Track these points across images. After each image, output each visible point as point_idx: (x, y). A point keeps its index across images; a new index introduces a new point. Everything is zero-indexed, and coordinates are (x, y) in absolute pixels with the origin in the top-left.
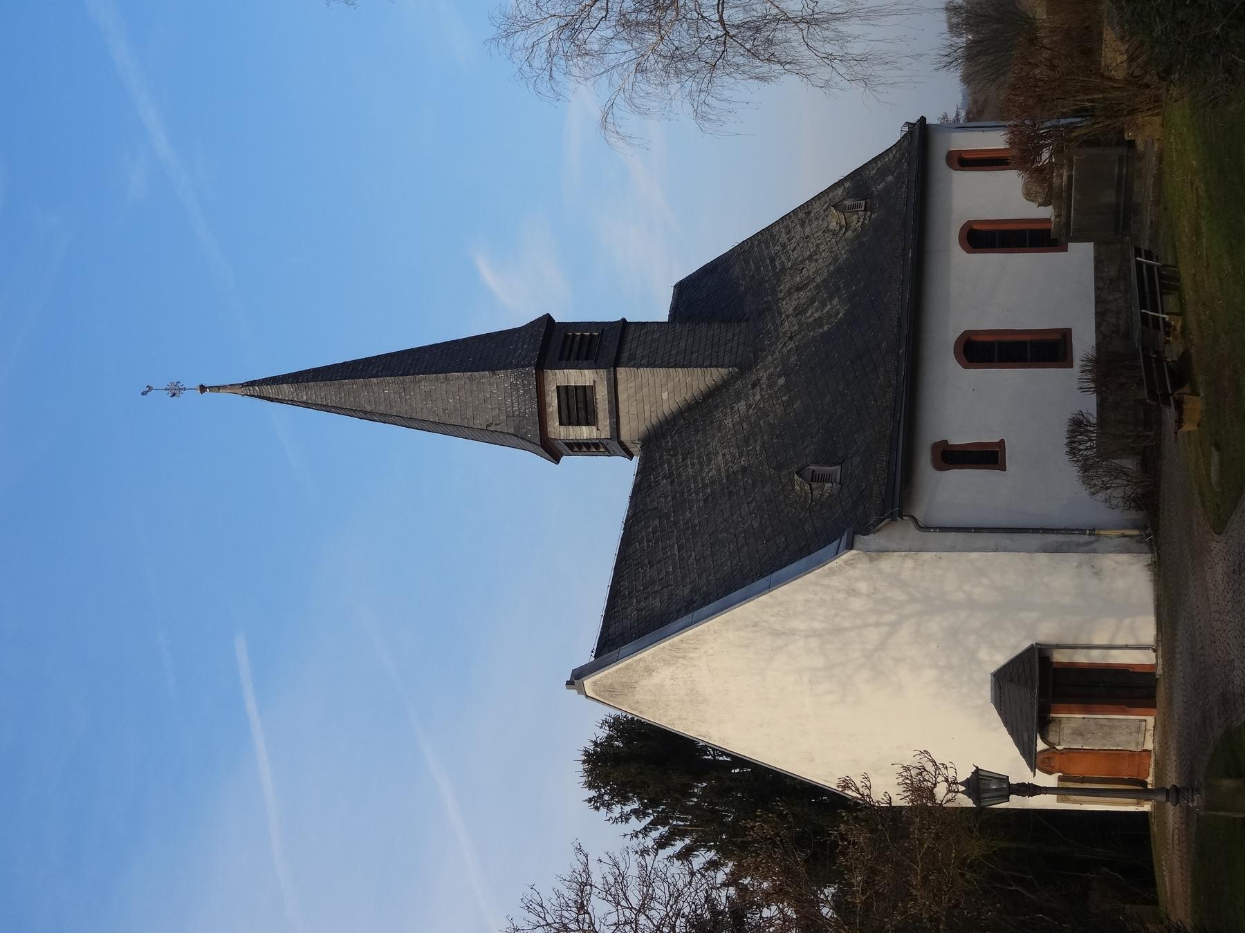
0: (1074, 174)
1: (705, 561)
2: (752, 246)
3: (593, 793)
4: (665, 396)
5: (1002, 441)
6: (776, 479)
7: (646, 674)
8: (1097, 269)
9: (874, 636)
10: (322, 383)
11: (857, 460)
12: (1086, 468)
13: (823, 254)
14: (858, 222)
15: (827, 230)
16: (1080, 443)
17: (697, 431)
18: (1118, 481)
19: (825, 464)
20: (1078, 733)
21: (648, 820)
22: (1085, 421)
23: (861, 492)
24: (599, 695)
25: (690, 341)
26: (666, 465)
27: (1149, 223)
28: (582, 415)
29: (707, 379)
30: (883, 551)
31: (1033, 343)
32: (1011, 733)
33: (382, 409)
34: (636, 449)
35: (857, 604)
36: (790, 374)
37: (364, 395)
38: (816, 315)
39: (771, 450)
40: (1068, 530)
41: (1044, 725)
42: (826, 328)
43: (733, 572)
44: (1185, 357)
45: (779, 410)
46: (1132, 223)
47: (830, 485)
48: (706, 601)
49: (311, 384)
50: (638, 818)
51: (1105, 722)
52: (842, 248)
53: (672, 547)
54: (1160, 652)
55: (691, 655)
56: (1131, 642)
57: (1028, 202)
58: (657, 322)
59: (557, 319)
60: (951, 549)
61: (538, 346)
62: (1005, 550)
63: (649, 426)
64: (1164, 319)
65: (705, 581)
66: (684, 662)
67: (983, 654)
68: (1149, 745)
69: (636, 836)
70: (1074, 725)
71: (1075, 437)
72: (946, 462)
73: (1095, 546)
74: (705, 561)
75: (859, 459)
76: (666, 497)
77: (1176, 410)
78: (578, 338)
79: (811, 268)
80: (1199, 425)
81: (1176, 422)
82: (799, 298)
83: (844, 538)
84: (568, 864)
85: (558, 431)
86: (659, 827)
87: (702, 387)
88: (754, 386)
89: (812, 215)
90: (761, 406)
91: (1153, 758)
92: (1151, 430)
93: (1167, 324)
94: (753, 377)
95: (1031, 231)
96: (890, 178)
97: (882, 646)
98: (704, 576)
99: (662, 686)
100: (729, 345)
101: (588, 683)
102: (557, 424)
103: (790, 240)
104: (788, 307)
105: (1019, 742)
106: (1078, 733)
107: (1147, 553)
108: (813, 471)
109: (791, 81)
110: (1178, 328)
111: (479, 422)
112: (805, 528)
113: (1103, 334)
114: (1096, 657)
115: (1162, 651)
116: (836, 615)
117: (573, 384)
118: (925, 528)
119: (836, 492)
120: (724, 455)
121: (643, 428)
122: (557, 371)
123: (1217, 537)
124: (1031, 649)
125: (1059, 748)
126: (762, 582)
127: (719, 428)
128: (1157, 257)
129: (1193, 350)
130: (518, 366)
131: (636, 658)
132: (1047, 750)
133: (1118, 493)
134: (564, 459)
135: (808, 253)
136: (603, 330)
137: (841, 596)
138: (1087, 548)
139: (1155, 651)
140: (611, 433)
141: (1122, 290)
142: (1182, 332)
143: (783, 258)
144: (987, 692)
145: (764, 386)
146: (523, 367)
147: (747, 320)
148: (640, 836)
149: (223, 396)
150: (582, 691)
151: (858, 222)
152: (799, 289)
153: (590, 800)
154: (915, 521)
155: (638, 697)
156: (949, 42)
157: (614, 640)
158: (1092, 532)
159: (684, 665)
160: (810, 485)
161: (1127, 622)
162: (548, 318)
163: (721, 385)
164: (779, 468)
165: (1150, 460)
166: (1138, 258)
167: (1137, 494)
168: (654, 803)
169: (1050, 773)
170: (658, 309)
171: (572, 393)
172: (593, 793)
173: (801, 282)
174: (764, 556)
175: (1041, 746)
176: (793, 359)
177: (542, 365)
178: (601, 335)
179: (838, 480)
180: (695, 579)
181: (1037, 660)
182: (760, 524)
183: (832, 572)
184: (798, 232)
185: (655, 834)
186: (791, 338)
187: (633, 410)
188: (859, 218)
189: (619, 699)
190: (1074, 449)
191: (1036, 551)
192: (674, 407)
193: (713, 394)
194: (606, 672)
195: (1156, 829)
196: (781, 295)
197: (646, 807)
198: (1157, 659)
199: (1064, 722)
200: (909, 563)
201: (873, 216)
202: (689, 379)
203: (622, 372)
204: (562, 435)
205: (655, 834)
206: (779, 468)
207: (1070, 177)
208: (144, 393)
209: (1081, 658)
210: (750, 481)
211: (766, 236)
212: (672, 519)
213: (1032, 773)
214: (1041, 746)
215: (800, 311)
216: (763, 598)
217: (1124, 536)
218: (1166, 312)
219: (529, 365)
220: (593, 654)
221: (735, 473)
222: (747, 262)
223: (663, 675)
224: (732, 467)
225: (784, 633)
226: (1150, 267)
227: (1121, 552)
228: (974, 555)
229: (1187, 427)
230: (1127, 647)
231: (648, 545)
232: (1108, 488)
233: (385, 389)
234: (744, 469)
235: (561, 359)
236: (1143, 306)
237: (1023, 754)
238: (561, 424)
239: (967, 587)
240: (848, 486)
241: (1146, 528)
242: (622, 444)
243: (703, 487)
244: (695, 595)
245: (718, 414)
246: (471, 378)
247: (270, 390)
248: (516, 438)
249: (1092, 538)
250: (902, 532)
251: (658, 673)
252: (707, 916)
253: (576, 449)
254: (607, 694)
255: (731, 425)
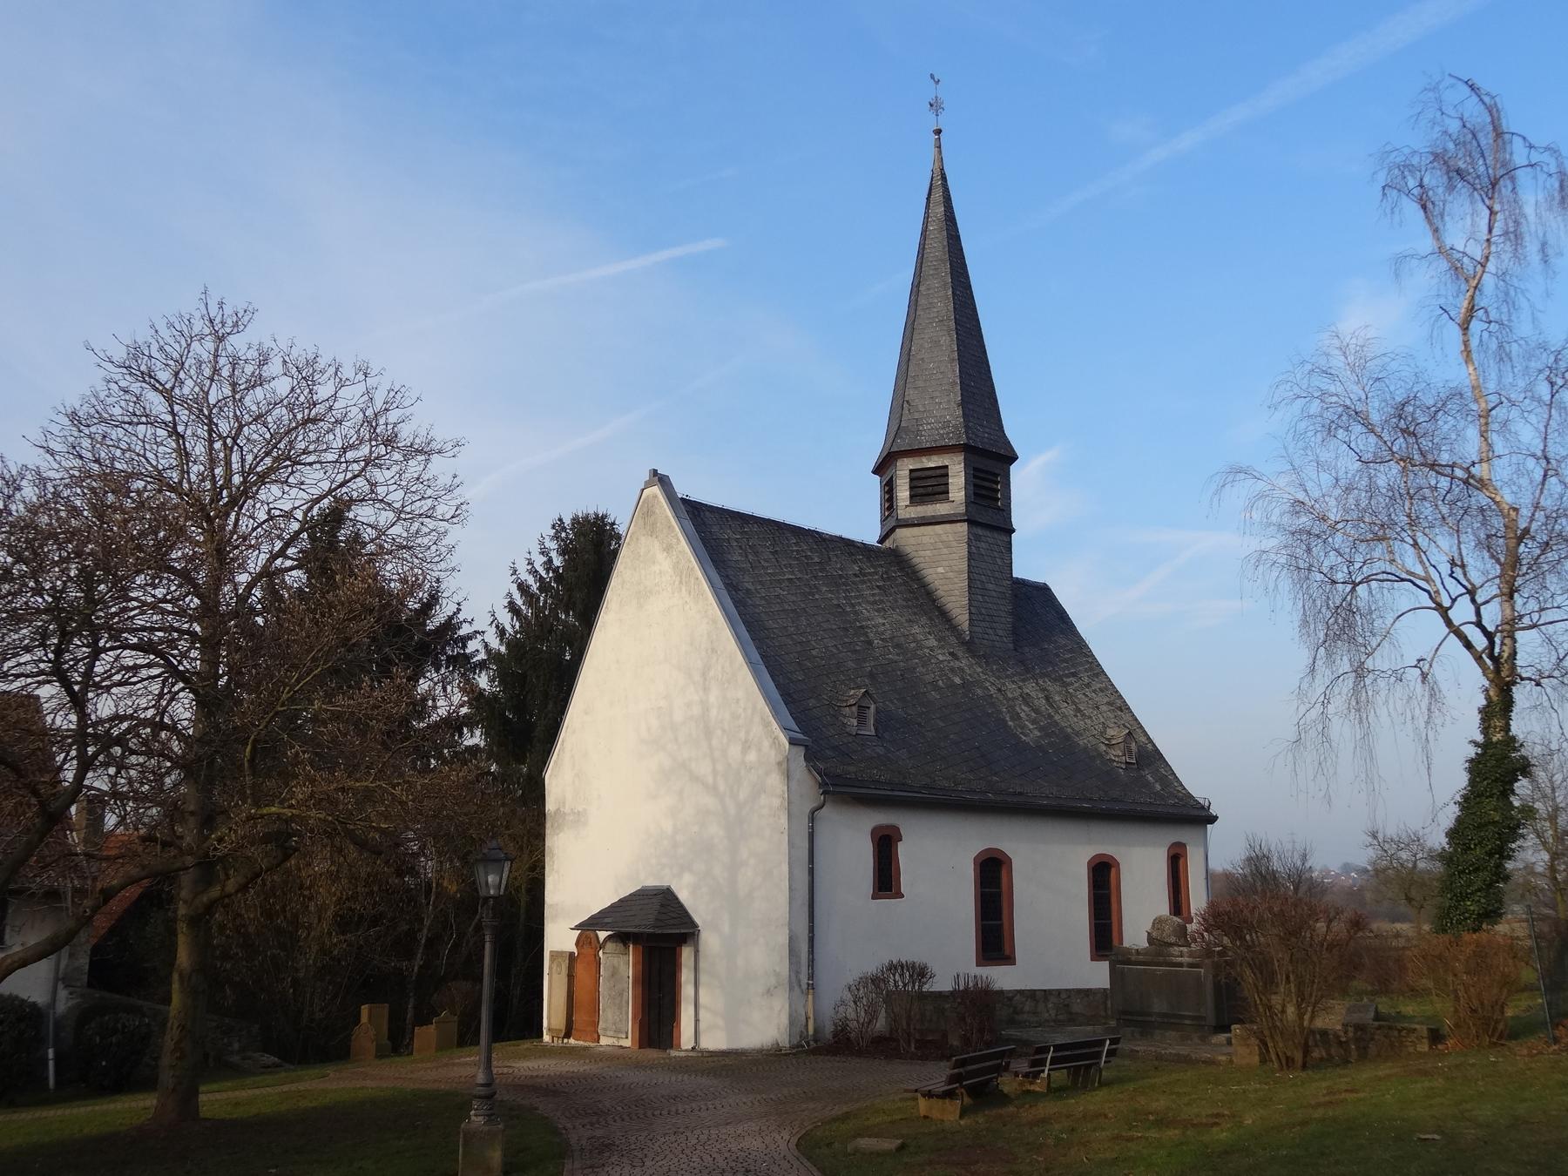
0: (1184, 969)
1: (778, 603)
2: (1086, 656)
3: (567, 522)
4: (941, 570)
5: (900, 895)
6: (860, 673)
7: (664, 546)
8: (1079, 991)
9: (704, 768)
10: (945, 243)
11: (881, 751)
12: (876, 981)
13: (1082, 723)
14: (1115, 756)
15: (1105, 727)
16: (902, 975)
17: (906, 600)
18: (863, 1014)
19: (876, 720)
20: (614, 973)
21: (543, 574)
22: (925, 980)
23: (847, 755)
24: (642, 506)
25: (994, 594)
26: (873, 570)
27: (1138, 1048)
28: (921, 491)
29: (958, 610)
30: (788, 776)
31: (1000, 927)
32: (612, 906)
33: (922, 301)
34: (888, 544)
35: (735, 751)
36: (964, 687)
37: (936, 283)
38: (1022, 715)
39: (890, 669)
40: (813, 962)
41: (622, 938)
42: (1010, 723)
43: (767, 629)
44: (1004, 1099)
45: (929, 678)
46: (1132, 1028)
47: (856, 724)
48: (738, 603)
49: (945, 233)
50: (545, 563)
51: (625, 998)
52: (1088, 741)
53: (792, 573)
54: (691, 1054)
55: (684, 589)
56: (702, 1026)
57: (1152, 921)
58: (1011, 563)
59: (1013, 468)
60: (791, 844)
61: (987, 447)
62: (791, 898)
63: (910, 556)
64: (1043, 1071)
65: (758, 603)
66: (677, 583)
67: (687, 878)
68: (604, 1041)
69: (529, 564)
70: (622, 967)
71: (908, 970)
72: (881, 838)
73: (797, 988)
74: (778, 603)
75: (881, 753)
76: (841, 569)
77: (943, 1091)
78: (995, 479)
79: (1068, 710)
80: (926, 1117)
81: (930, 1091)
82: (1039, 699)
83: (801, 736)
84: (441, 435)
85: (903, 470)
86: (538, 584)
87: (949, 606)
88: (951, 654)
89: (1119, 713)
90: (933, 661)
91: (592, 1045)
92: (915, 1048)
93: (1036, 1075)
94: (960, 654)
95: (1110, 925)
96: (1158, 787)
97: (695, 778)
98: (763, 602)
99: (654, 562)
100: (990, 631)
101: (656, 490)
102: (911, 467)
103: (1094, 691)
104: (1030, 688)
105: (603, 913)
106: (614, 973)
107: (790, 1042)
108: (869, 708)
109: (1303, 657)
110: (1032, 1088)
111: (911, 394)
112: (812, 700)
113: (1013, 997)
114: (687, 990)
115: (692, 1057)
116: (724, 731)
117: (950, 481)
118: (812, 818)
119: (848, 730)
120: (884, 624)
121: (908, 550)
122: (963, 465)
123: (794, 1140)
124: (694, 925)
125: (601, 952)
126: (756, 656)
127: (910, 621)
128: (1110, 1062)
129: (1011, 1109)
130: (967, 427)
131: (680, 535)
132: (598, 941)
133: (851, 1014)
134: (877, 478)
135: (1083, 709)
136: (1003, 510)
137: (742, 735)
138: (794, 981)
139: (693, 1048)
140: (903, 519)
141: (1058, 1017)
142: (1028, 1091)
143: (1077, 685)
144: (652, 882)
145: (952, 664)
146: (966, 432)
147: (1015, 650)
148: (529, 567)
149: (932, 151)
150: (648, 485)
151: (1115, 756)
152: (1047, 698)
153: (560, 520)
154: (821, 807)
155: (643, 539)
156: (1273, 849)
157: (699, 516)
158: (811, 987)
159: (674, 582)
160: (855, 704)
161: (721, 1023)
162: (1013, 458)
163: (952, 624)
164: (872, 676)
165: (884, 1047)
166: (1108, 1042)
167: (850, 1033)
168: (559, 578)
169: (577, 944)
170: (1025, 567)
171: (942, 480)
172: (567, 522)
173: (1055, 702)
174: (783, 660)
175: (602, 935)
176: (979, 692)
177: (968, 450)
178: (999, 509)
179: (859, 732)
180: (759, 593)
181: (683, 931)
182: (815, 657)
183: (766, 725)
184: (1102, 699)
185: (531, 580)
186: (999, 690)
187: (926, 540)
188: (1118, 756)
189: (641, 522)
190: (896, 968)
191: (790, 930)
192: (929, 579)
193: (945, 614)
194: (666, 506)
195: (525, 1046)
196: (1041, 682)
197: (556, 570)
198: (686, 1051)
199: (625, 957)
200: (776, 802)
201: (1121, 770)
202: (957, 592)
203: (965, 526)
204: (900, 472)
205: (531, 580)
206: (872, 676)
207: (1180, 965)
208: (932, 76)
209: (686, 976)
210: (858, 648)
211: (1096, 671)
212: (820, 574)
213: (573, 927)
214: (602, 935)
215: (1026, 699)
216: (740, 658)
217: (807, 1019)
218: (1051, 1072)
219: (968, 438)
220: (684, 497)
221: (866, 634)
222: (1071, 651)
223: (664, 563)
224: (871, 632)
225: (705, 679)
226: (1098, 1055)
227: (790, 1016)
228: (785, 868)
229: (923, 1104)
230: (697, 1021)
231: (793, 551)
232: (855, 1002)
233: (941, 303)
234: (870, 643)
235: (975, 469)
236: (1058, 1048)
237: (592, 918)
238: (911, 471)
239: (752, 861)
240: (854, 741)
241: (816, 1041)
242: (892, 530)
243: (852, 604)
244: (744, 593)
245: (924, 620)
246: (954, 383)
247: (938, 195)
248: (896, 429)
249: (804, 987)
250: (809, 790)
251: (666, 558)
252: (462, 632)
253: (887, 488)
254: (645, 510)
255: (913, 631)
